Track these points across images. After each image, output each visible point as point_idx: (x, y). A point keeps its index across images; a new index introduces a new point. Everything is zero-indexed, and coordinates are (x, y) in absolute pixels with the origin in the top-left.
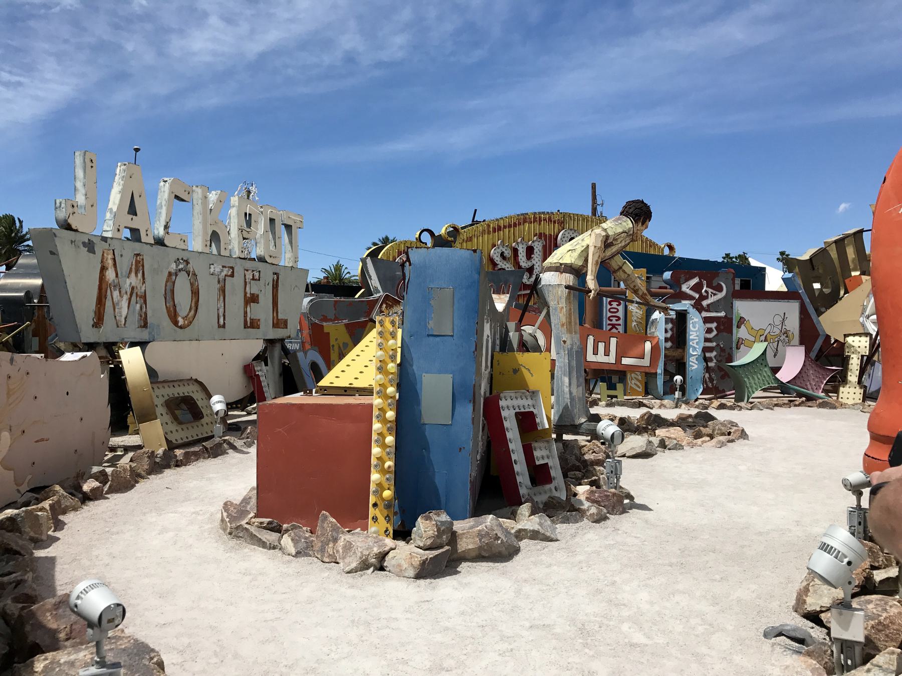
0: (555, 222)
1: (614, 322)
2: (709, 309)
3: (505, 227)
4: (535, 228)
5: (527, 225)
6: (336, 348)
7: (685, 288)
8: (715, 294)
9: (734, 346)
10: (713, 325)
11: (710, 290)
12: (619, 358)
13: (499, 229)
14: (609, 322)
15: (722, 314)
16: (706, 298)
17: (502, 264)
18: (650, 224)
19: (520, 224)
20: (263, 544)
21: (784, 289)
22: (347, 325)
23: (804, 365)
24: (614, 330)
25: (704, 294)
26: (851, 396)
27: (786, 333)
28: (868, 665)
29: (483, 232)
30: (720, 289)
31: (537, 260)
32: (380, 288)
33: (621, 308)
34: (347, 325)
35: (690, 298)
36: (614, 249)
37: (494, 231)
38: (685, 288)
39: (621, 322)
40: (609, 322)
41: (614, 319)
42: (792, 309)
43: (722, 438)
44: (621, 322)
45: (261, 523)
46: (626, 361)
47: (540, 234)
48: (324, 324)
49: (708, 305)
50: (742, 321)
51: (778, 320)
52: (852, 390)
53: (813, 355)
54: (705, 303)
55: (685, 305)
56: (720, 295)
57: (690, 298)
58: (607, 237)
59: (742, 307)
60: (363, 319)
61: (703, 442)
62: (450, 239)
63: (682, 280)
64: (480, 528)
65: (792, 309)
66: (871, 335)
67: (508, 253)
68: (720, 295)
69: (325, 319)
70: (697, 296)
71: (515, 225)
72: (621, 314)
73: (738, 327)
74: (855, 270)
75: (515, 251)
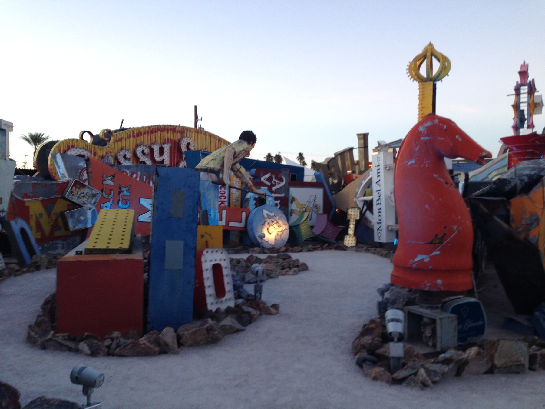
0: (177, 132)
1: (223, 200)
2: (276, 192)
3: (144, 133)
4: (166, 135)
5: (159, 132)
6: (34, 217)
7: (263, 179)
8: (279, 184)
9: (289, 214)
10: (278, 202)
11: (277, 181)
12: (227, 222)
13: (141, 134)
14: (220, 200)
15: (283, 195)
16: (274, 185)
17: (143, 158)
18: (256, 145)
19: (155, 132)
20: (70, 349)
21: (315, 181)
22: (42, 201)
23: (327, 225)
24: (222, 205)
25: (273, 183)
26: (350, 242)
27: (316, 206)
28: (405, 367)
29: (130, 136)
30: (282, 180)
31: (166, 156)
32: (66, 175)
33: (227, 191)
34: (42, 201)
35: (265, 185)
36: (237, 159)
37: (137, 136)
38: (263, 179)
39: (226, 200)
40: (220, 200)
41: (223, 198)
42: (319, 192)
43: (296, 269)
44: (226, 200)
45: (64, 336)
46: (232, 224)
47: (168, 139)
48: (25, 200)
49: (276, 190)
50: (293, 199)
51: (312, 199)
52: (351, 239)
53: (330, 218)
54: (274, 188)
55: (263, 190)
56: (282, 184)
57: (265, 185)
58: (235, 153)
59: (294, 192)
60: (54, 196)
61: (287, 272)
62: (106, 139)
63: (261, 175)
64: (206, 326)
65: (319, 192)
66: (359, 208)
67: (147, 151)
68: (282, 184)
69: (26, 196)
70: (269, 184)
71: (151, 133)
72: (226, 195)
73: (292, 203)
74: (349, 170)
75: (152, 150)
